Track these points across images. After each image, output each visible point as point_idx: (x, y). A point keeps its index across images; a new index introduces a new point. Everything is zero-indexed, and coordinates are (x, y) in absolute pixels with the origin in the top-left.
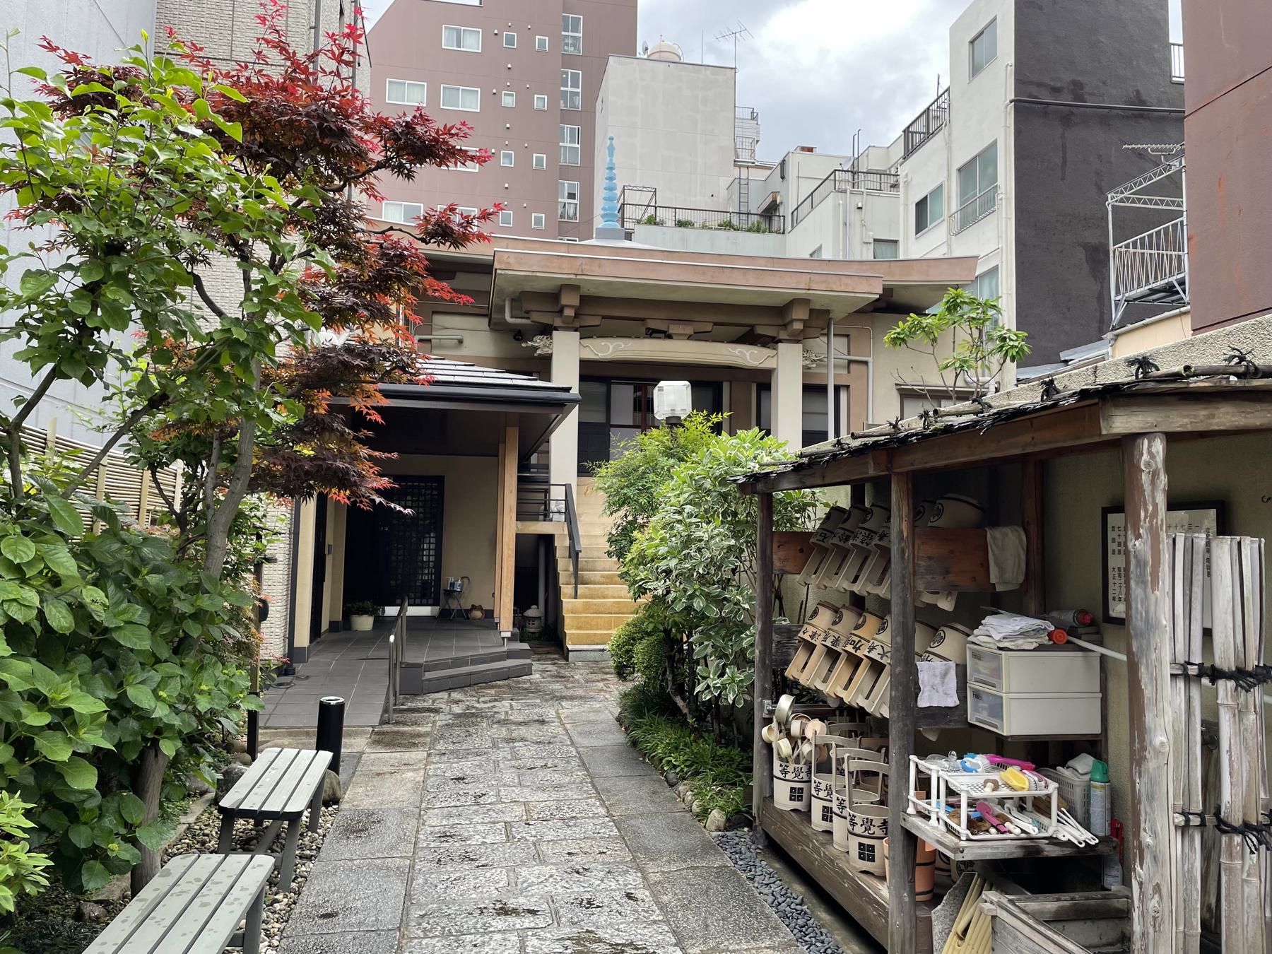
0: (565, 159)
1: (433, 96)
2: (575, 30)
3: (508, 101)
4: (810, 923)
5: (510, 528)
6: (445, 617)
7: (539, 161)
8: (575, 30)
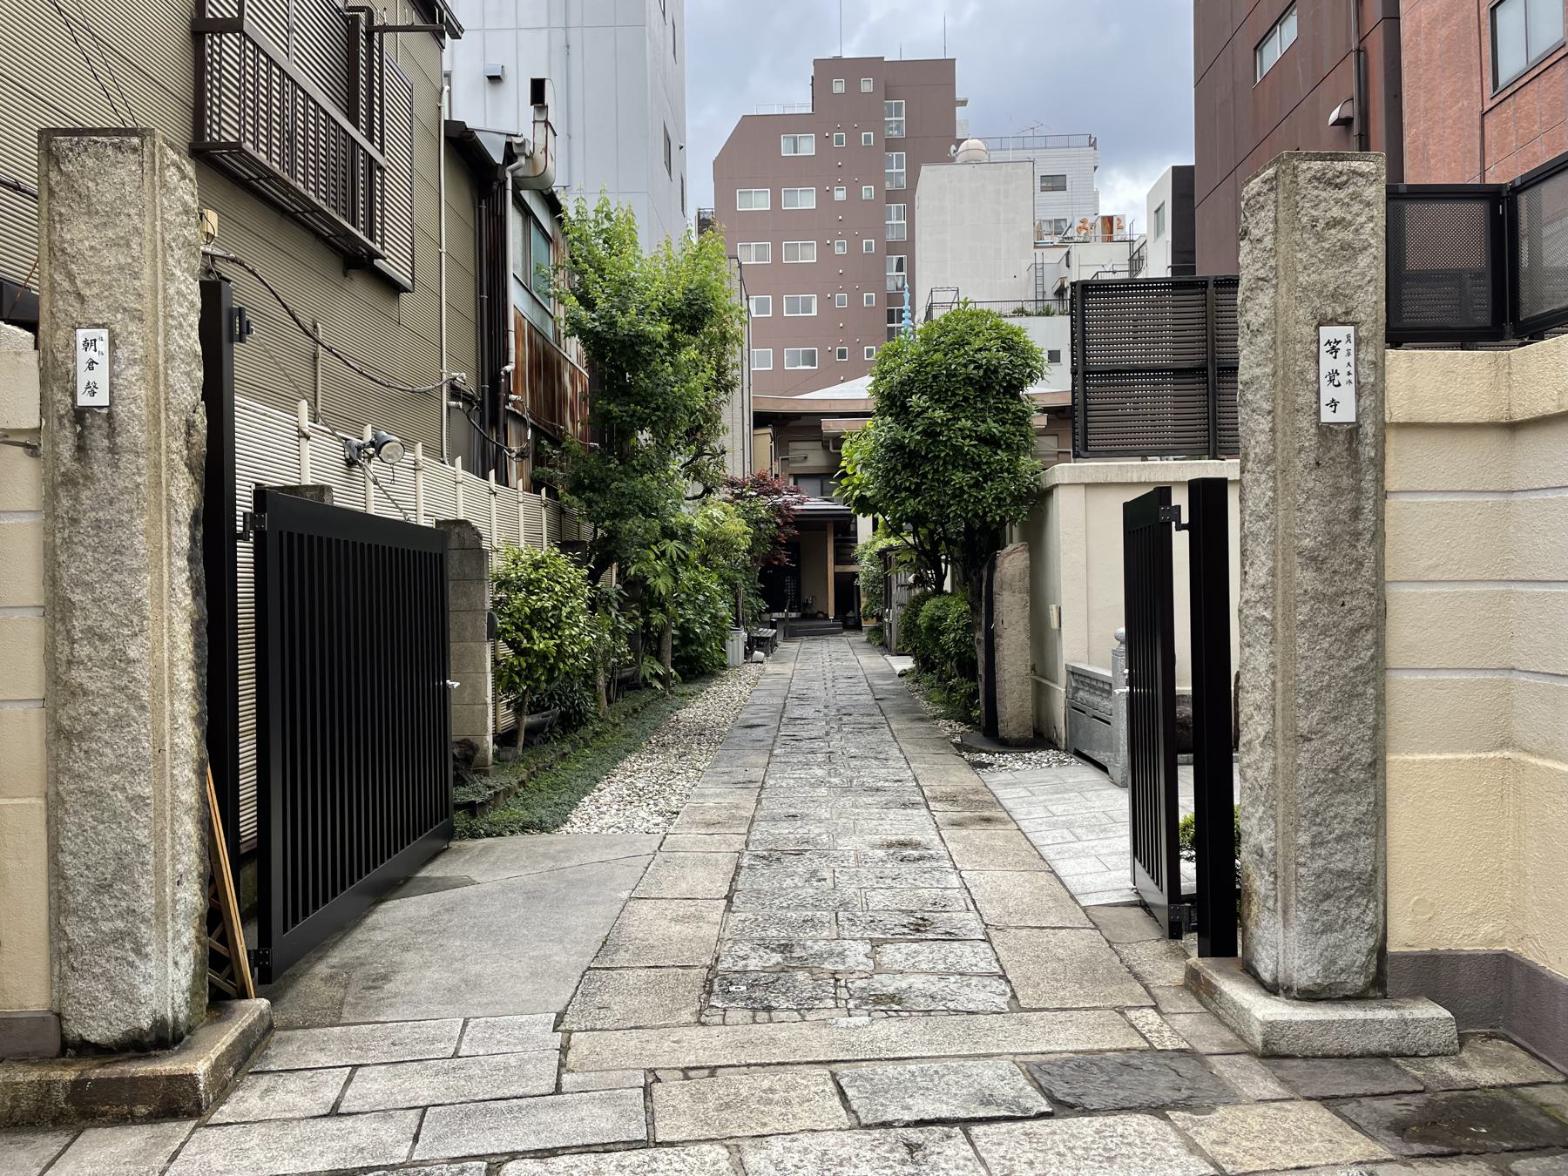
1: (776, 200)
3: (840, 195)
4: (1504, 865)
5: (831, 569)
6: (804, 617)
7: (869, 246)
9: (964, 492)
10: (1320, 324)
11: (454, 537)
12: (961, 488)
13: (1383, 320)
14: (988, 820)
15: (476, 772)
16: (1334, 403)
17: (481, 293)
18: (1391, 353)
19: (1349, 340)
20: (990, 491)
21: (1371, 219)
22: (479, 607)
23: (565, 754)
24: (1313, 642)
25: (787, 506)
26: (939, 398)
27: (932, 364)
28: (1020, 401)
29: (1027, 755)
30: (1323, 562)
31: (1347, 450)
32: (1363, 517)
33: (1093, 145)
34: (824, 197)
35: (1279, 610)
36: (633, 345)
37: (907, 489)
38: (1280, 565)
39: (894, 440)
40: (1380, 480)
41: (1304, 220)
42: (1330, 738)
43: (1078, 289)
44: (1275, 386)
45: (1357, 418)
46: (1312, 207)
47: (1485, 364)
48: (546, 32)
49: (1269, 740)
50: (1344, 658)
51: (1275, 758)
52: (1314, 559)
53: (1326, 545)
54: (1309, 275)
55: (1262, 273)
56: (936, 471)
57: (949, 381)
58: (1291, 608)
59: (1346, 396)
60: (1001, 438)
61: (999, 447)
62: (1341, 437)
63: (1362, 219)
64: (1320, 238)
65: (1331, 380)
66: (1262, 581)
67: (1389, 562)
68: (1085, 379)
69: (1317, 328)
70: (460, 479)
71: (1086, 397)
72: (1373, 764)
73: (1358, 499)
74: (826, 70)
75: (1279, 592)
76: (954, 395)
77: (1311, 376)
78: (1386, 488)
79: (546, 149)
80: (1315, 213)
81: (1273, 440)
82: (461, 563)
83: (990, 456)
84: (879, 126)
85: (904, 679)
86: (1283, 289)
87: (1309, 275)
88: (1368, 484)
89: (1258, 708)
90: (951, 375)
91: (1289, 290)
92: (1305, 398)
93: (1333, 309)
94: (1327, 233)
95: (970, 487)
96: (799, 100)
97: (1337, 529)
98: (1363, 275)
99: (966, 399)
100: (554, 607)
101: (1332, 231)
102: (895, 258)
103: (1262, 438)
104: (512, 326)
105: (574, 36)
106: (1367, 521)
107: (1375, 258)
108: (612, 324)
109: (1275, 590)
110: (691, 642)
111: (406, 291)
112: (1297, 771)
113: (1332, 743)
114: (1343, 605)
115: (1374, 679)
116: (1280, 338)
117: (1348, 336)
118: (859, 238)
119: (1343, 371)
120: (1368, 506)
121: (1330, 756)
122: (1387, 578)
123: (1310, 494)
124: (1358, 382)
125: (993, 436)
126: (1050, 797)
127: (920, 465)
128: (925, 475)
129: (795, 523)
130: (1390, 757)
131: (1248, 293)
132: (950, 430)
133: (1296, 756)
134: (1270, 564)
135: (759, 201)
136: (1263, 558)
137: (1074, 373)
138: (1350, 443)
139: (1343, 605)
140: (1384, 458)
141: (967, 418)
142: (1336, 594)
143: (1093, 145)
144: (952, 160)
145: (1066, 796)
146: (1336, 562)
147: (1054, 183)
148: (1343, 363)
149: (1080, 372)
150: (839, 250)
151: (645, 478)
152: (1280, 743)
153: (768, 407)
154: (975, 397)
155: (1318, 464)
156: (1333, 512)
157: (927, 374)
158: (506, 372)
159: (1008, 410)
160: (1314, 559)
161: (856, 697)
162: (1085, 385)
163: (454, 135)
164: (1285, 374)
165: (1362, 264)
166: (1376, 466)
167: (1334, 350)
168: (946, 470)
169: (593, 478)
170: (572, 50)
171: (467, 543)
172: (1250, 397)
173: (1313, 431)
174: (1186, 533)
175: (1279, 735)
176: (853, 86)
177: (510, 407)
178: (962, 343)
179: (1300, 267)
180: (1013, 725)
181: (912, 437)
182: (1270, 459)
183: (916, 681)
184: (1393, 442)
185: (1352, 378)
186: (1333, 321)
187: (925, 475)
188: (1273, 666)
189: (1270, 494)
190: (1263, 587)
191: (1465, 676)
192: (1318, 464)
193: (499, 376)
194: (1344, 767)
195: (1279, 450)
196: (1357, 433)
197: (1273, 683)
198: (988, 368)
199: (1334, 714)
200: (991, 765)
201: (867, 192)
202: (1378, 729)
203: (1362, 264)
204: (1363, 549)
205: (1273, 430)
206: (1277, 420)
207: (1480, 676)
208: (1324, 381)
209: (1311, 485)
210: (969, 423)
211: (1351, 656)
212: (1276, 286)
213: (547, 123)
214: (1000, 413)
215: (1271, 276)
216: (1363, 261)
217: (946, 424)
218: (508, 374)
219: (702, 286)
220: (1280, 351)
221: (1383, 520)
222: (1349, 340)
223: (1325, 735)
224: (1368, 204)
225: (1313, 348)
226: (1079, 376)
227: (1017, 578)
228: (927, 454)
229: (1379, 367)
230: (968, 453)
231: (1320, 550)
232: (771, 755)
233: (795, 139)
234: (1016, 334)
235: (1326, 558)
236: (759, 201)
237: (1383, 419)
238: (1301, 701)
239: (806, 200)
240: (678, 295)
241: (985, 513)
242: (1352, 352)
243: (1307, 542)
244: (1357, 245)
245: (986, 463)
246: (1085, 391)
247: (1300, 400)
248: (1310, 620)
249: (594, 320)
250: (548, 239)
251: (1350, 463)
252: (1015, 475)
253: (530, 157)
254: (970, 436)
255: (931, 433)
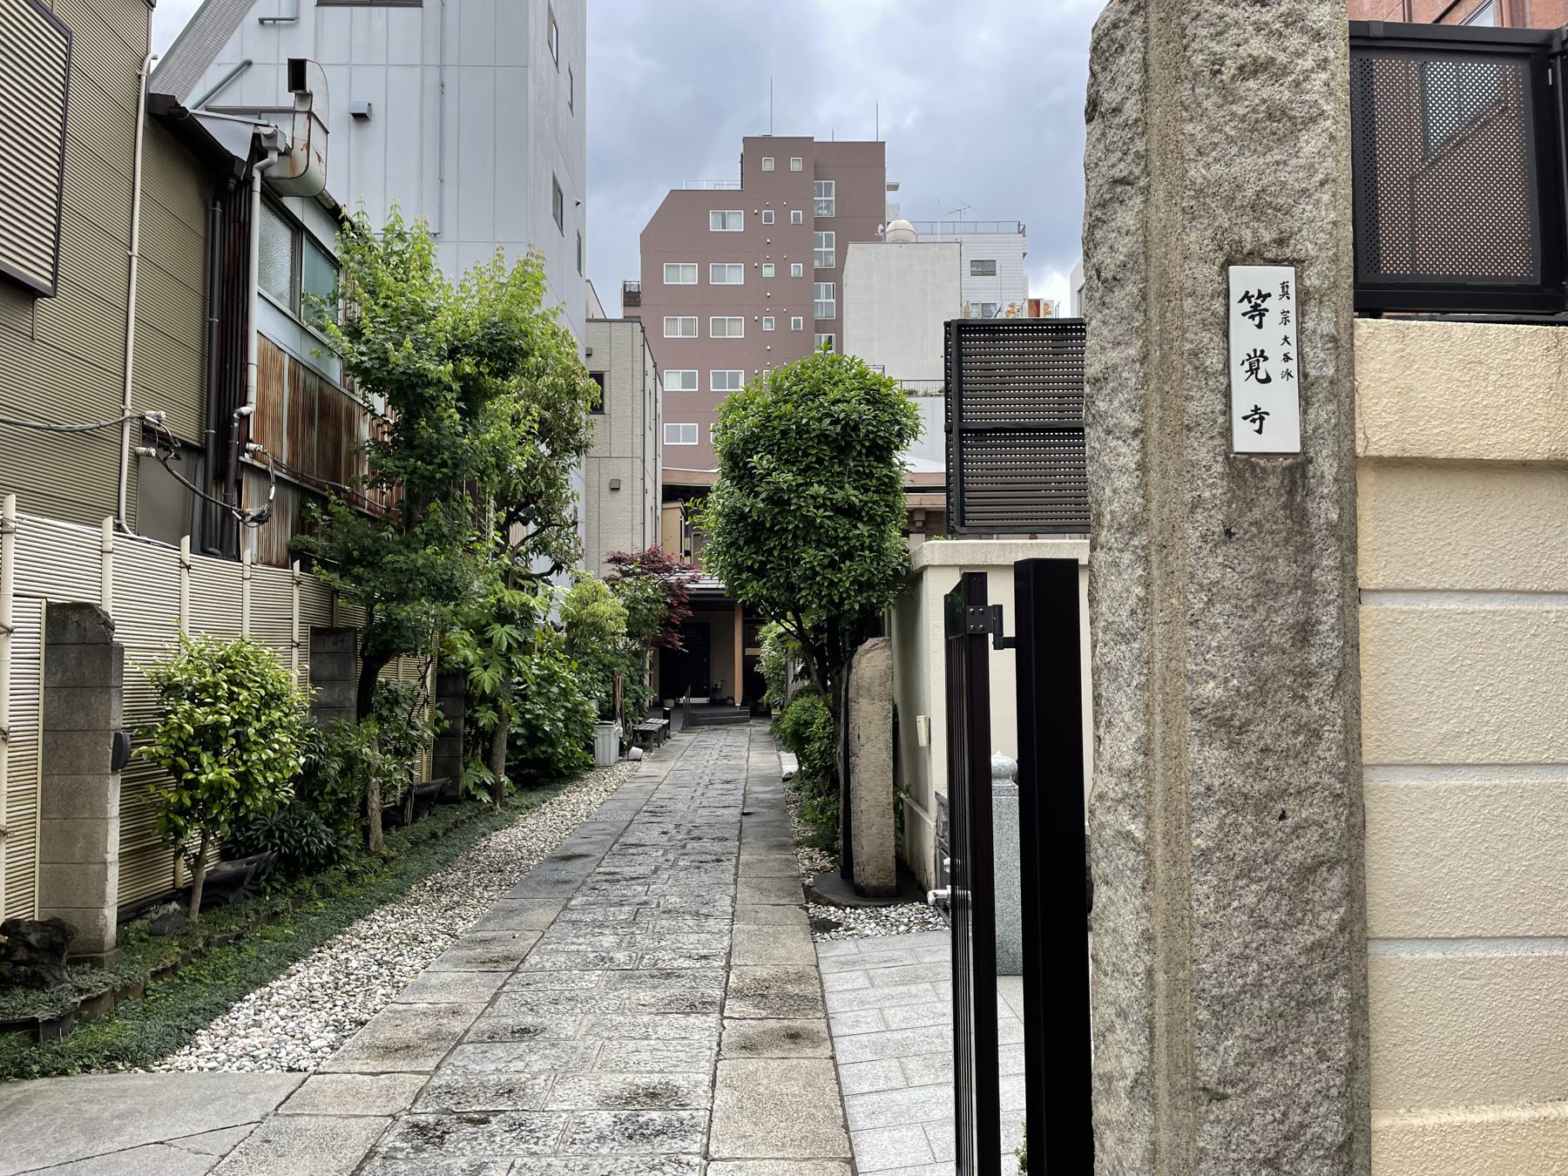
0: (820, 315)
1: (704, 275)
2: (828, 194)
7: (797, 323)
8: (828, 194)
9: (817, 574)
10: (1229, 262)
11: (72, 627)
12: (813, 568)
13: (1348, 260)
14: (794, 1036)
15: (74, 962)
16: (1258, 415)
17: (211, 316)
18: (1365, 325)
19: (1285, 294)
20: (848, 573)
21: (1323, 64)
22: (102, 725)
23: (276, 914)
24: (1224, 893)
25: (680, 585)
26: (787, 459)
27: (780, 418)
28: (891, 465)
29: (884, 911)
30: (1242, 730)
31: (1285, 507)
32: (1317, 640)
33: (1022, 232)
34: (753, 273)
35: (1159, 826)
36: (413, 386)
37: (750, 569)
38: (1158, 731)
39: (734, 510)
40: (1348, 568)
41: (1198, 60)
42: (1262, 1093)
43: (953, 329)
44: (1145, 381)
45: (1303, 443)
46: (1212, 37)
47: (1539, 350)
48: (418, 70)
49: (1142, 1086)
50: (1287, 927)
51: (1154, 1129)
52: (1223, 723)
53: (1248, 696)
54: (1207, 166)
55: (1121, 171)
56: (784, 547)
57: (801, 438)
58: (1179, 821)
59: (1282, 399)
60: (862, 509)
61: (860, 519)
62: (1273, 481)
63: (1308, 63)
64: (1228, 95)
65: (1253, 370)
66: (1126, 763)
67: (1369, 727)
68: (961, 438)
69: (1224, 268)
70: (109, 546)
71: (962, 460)
72: (1346, 1146)
73: (1308, 605)
74: (755, 148)
75: (1158, 788)
76: (806, 455)
77: (1213, 361)
78: (1360, 583)
79: (308, 146)
80: (1217, 48)
81: (1143, 485)
82: (79, 663)
83: (849, 530)
84: (808, 206)
85: (788, 784)
86: (1159, 195)
87: (1207, 166)
88: (1326, 575)
89: (1123, 1014)
90: (802, 431)
91: (1170, 195)
92: (1203, 403)
93: (1255, 232)
94: (1242, 87)
95: (824, 567)
96: (727, 176)
97: (1268, 663)
98: (1311, 169)
99: (820, 461)
100: (235, 723)
101: (1251, 84)
102: (824, 337)
103: (1124, 482)
104: (254, 357)
105: (450, 76)
106: (1325, 650)
107: (1332, 138)
108: (385, 361)
109: (1150, 781)
110: (541, 741)
111: (43, 295)
112: (1198, 1161)
113: (1265, 1103)
114: (1283, 817)
115: (1347, 968)
116: (1154, 287)
117: (1284, 286)
118: (788, 315)
119: (1275, 352)
120: (1328, 618)
121: (1263, 1132)
122: (1367, 758)
123: (1213, 592)
124: (1303, 375)
125: (851, 506)
126: (893, 991)
127: (766, 539)
128: (770, 552)
129: (690, 603)
130: (1381, 1122)
131: (1098, 213)
132: (799, 497)
133: (1195, 1130)
134: (1142, 729)
135: (687, 275)
136: (1128, 716)
137: (948, 431)
138: (1291, 493)
139: (1283, 817)
140: (1354, 523)
141: (820, 483)
142: (1269, 796)
143: (1022, 232)
144: (879, 240)
145: (913, 989)
146: (1266, 730)
147: (984, 268)
148: (1275, 336)
149: (955, 429)
150: (767, 327)
151: (428, 551)
152: (1164, 1100)
153: (679, 480)
154: (832, 458)
155: (1228, 533)
156: (1260, 629)
157: (774, 428)
158: (241, 415)
159: (871, 475)
160: (1223, 723)
161: (720, 812)
162: (962, 446)
163: (161, 111)
164: (1164, 357)
165: (1307, 150)
166: (1340, 539)
167: (1257, 313)
168: (796, 546)
169: (363, 549)
170: (447, 89)
171: (90, 634)
172: (1102, 405)
173: (1218, 468)
174: (1011, 653)
175: (1161, 1081)
176: (782, 164)
177: (247, 458)
178: (816, 393)
179: (1189, 151)
180: (870, 869)
181: (756, 505)
182: (1138, 523)
183: (797, 789)
184: (1372, 495)
185: (1292, 366)
186: (1253, 257)
187: (770, 552)
188: (1147, 936)
189: (1139, 590)
190: (1129, 774)
191: (1516, 951)
192: (1228, 533)
193: (231, 420)
194: (1291, 1154)
195: (1154, 506)
196: (1304, 476)
197: (1150, 972)
198: (847, 424)
199: (1269, 1042)
200: (838, 925)
201: (796, 270)
202: (1356, 1069)
203: (1307, 150)
204: (1320, 703)
205: (1142, 467)
206: (1151, 447)
207: (1542, 951)
208: (1239, 372)
209: (1215, 574)
210: (823, 489)
211: (1300, 922)
212: (1146, 190)
213: (310, 114)
214: (861, 479)
215: (1137, 172)
216: (1310, 143)
217: (796, 489)
218: (245, 418)
219: (508, 318)
220: (1154, 313)
221: (1356, 646)
222: (1285, 294)
223: (1252, 1087)
224: (1318, 36)
225: (1218, 305)
226: (955, 435)
227: (877, 682)
228: (773, 525)
229: (1342, 347)
230: (821, 526)
231: (1235, 705)
232: (565, 908)
233: (724, 215)
234: (886, 386)
235: (1249, 722)
236: (687, 275)
237: (1353, 449)
238: (1203, 1015)
239: (734, 276)
240: (473, 325)
241: (842, 600)
242: (1292, 317)
243: (1210, 690)
244: (1299, 112)
245: (844, 538)
246: (961, 453)
247: (1192, 407)
248: (1219, 848)
249: (362, 354)
250: (335, 263)
251: (1290, 532)
252: (880, 553)
253: (286, 153)
254: (823, 505)
255: (777, 500)
